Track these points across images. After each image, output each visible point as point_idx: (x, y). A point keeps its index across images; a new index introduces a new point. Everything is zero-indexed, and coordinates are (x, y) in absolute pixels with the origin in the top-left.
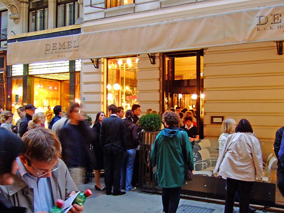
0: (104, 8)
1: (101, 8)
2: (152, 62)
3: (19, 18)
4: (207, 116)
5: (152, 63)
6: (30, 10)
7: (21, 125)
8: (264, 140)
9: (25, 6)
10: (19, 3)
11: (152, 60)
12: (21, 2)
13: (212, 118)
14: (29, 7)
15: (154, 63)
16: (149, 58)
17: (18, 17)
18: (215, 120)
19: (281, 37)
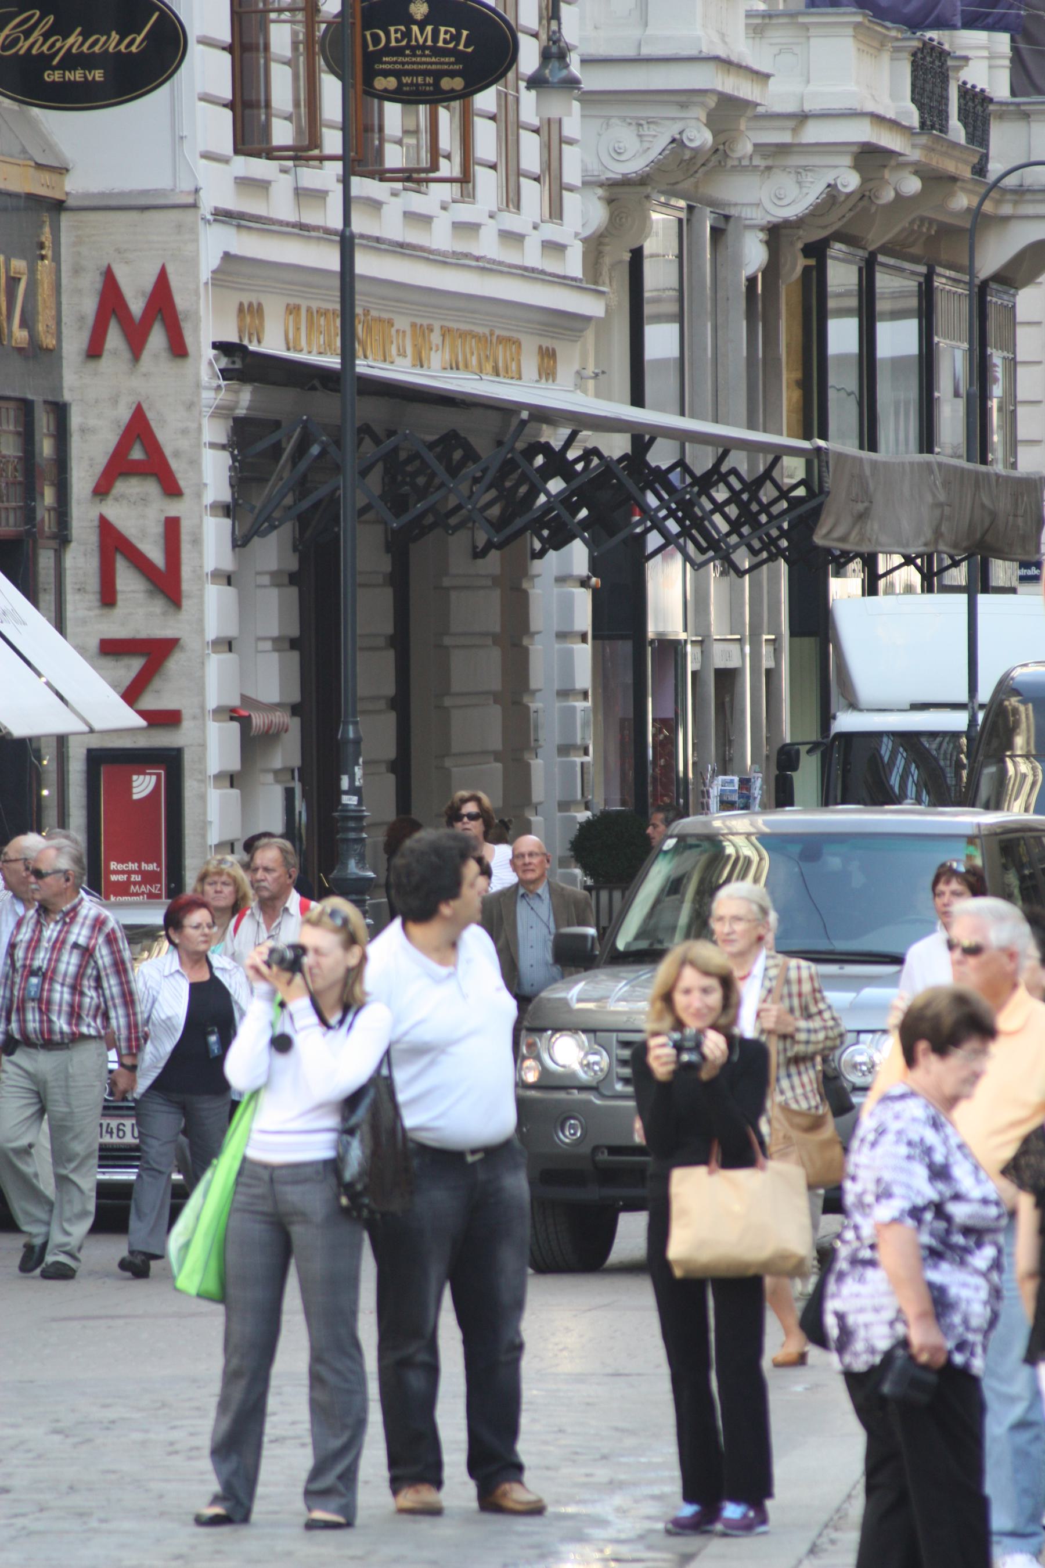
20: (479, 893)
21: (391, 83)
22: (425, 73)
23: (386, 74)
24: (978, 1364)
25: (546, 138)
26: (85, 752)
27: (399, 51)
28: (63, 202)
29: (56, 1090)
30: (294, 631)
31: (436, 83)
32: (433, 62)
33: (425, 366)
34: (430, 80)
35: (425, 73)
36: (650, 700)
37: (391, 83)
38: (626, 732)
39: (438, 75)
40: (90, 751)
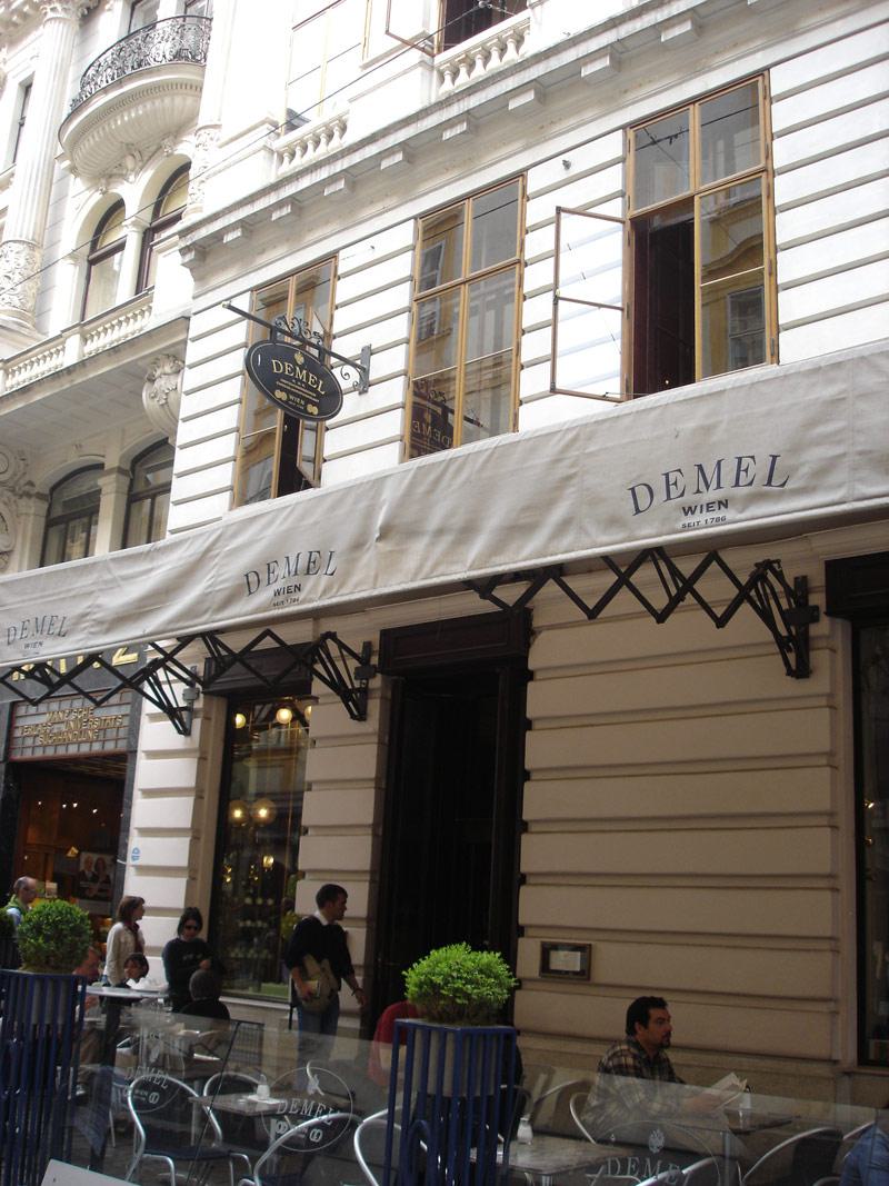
0: (618, 396)
1: (604, 398)
2: (794, 667)
3: (11, 551)
4: (531, 941)
5: (790, 672)
6: (50, 523)
7: (356, 713)
8: (737, 1059)
9: (32, 511)
10: (13, 498)
11: (792, 657)
12: (21, 496)
13: (547, 950)
14: (49, 511)
15: (801, 671)
16: (776, 649)
17: (7, 547)
18: (560, 960)
19: (520, 940)
20: (134, 224)
21: (283, 396)
22: (302, 398)
23: (282, 389)
24: (351, 405)
25: (601, 936)
26: (789, 678)
27: (289, 378)
28: (369, 347)
29: (92, 142)
30: (90, 184)
31: (305, 406)
32: (311, 395)
33: (285, 295)
34: (303, 402)
35: (302, 398)
36: (407, 1021)
37: (283, 396)
38: (199, 884)
39: (308, 401)
40: (718, 627)
